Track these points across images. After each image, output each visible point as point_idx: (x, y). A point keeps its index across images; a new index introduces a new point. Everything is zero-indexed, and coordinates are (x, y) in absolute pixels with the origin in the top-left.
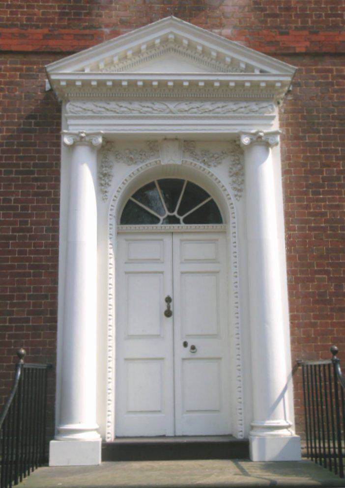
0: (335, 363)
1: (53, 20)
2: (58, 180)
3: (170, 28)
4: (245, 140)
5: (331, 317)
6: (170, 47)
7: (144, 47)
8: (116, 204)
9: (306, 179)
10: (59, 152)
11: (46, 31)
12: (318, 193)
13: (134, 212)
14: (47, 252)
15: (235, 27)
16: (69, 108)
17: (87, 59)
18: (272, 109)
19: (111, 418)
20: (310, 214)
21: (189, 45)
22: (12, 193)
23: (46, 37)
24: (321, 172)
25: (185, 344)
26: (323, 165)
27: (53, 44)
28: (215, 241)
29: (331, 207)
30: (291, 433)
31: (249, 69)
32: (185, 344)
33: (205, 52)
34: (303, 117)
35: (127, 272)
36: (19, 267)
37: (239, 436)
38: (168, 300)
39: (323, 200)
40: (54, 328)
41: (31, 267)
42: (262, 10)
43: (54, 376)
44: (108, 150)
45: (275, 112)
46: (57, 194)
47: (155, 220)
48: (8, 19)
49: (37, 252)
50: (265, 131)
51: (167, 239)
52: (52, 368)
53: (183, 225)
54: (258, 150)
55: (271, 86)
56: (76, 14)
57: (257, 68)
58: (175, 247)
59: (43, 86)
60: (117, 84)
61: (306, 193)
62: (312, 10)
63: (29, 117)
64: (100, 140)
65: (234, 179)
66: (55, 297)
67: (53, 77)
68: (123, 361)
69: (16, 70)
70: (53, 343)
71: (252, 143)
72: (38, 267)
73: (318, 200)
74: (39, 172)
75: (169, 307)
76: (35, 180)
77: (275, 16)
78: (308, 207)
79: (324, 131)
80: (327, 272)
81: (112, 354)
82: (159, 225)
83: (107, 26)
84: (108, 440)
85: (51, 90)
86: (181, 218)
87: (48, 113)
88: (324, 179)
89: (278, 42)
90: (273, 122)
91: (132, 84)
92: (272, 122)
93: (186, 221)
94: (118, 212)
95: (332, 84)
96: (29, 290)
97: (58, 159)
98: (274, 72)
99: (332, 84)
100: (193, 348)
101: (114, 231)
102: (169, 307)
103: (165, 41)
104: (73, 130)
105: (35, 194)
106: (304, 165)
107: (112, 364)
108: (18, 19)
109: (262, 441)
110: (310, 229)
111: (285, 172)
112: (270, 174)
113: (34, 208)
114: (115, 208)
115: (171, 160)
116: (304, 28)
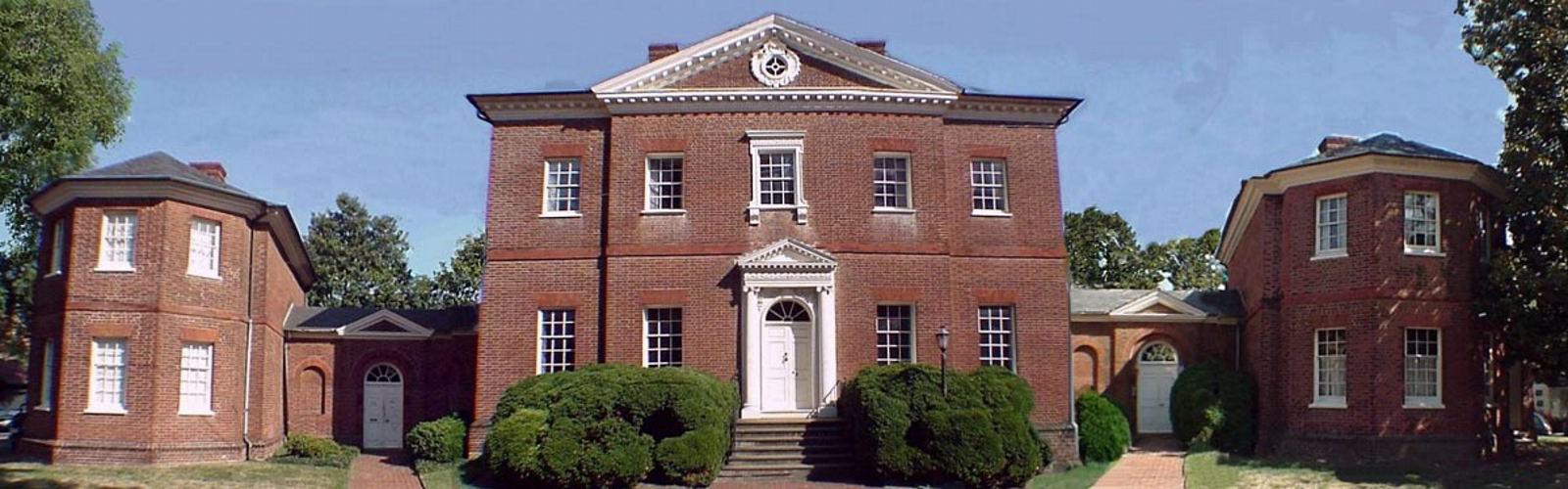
23: (726, 247)
47: (780, 319)
77: (825, 234)
112: (829, 303)
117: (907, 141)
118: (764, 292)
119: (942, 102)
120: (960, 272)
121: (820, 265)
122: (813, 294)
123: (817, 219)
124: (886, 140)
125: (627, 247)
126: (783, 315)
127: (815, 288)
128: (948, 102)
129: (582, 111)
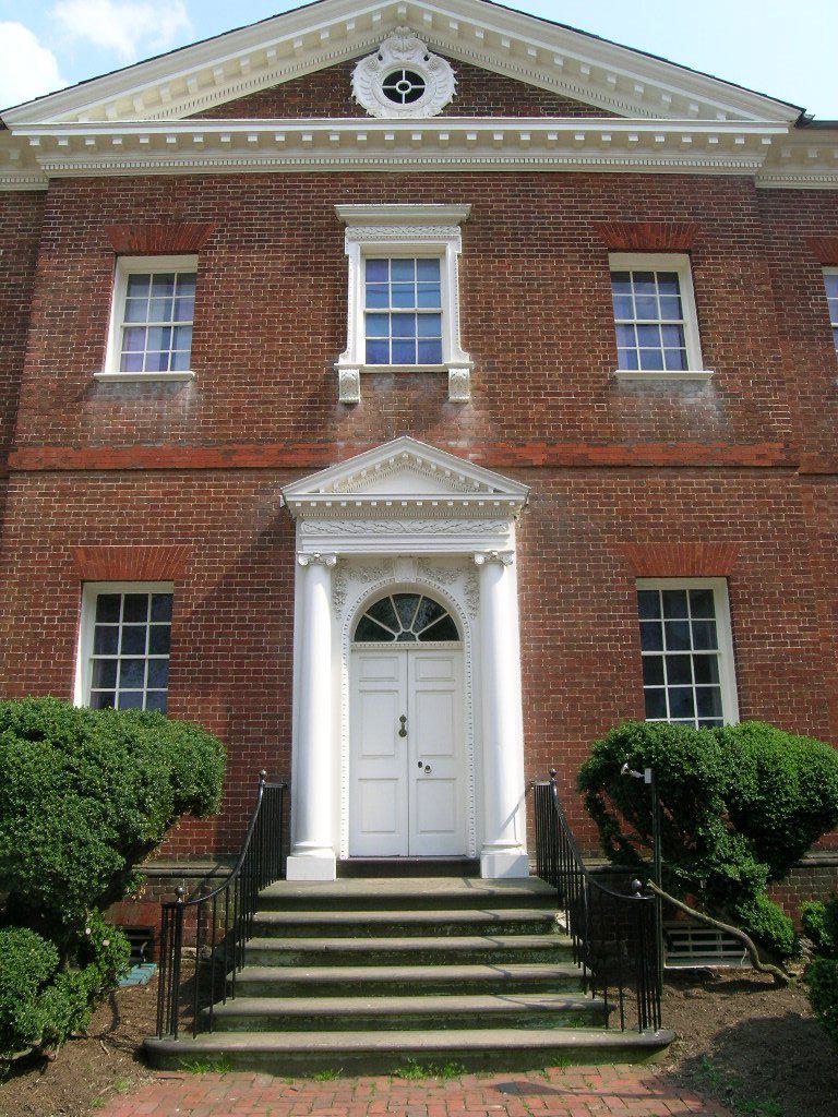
0: (553, 784)
1: (288, 434)
2: (292, 598)
3: (406, 446)
4: (479, 560)
5: (565, 738)
6: (404, 465)
7: (377, 467)
8: (350, 623)
9: (543, 596)
10: (293, 569)
11: (281, 446)
12: (555, 611)
13: (373, 627)
14: (280, 672)
15: (471, 439)
16: (304, 528)
17: (321, 480)
18: (507, 527)
19: (345, 836)
20: (547, 632)
21: (423, 463)
22: (246, 612)
23: (281, 452)
24: (558, 589)
25: (420, 765)
26: (560, 582)
27: (288, 459)
28: (449, 659)
29: (568, 625)
30: (523, 851)
31: (483, 488)
32: (420, 765)
33: (439, 471)
34: (540, 532)
35: (362, 690)
36: (255, 687)
37: (472, 856)
38: (403, 719)
39: (560, 618)
40: (289, 748)
41: (266, 687)
42: (501, 421)
43: (289, 795)
44: (343, 568)
45: (511, 530)
46: (291, 612)
47: (390, 637)
48: (244, 435)
49: (270, 672)
50: (499, 550)
51: (402, 657)
52: (287, 787)
53: (418, 642)
54: (493, 569)
55: (504, 504)
56: (311, 428)
57: (722, 111)
58: (409, 664)
59: (278, 502)
60: (351, 504)
61: (542, 611)
62: (550, 421)
63: (263, 534)
64: (334, 561)
65: (468, 597)
66: (289, 717)
67: (288, 499)
68: (357, 781)
69: (251, 486)
70: (288, 762)
71: (486, 561)
72: (272, 687)
73: (554, 618)
74: (273, 591)
75: (403, 727)
76: (270, 598)
77: (512, 427)
78: (543, 625)
79: (562, 546)
80: (562, 692)
81: (346, 773)
82: (394, 642)
83: (341, 440)
84: (342, 859)
85: (286, 506)
86: (417, 635)
87: (283, 529)
88: (561, 596)
89: (515, 455)
90: (507, 541)
91: (366, 504)
92: (509, 539)
93: (423, 637)
94: (354, 621)
95: (570, 498)
96: (263, 709)
97: (293, 577)
98: (509, 492)
99: (570, 498)
100: (428, 768)
101: (348, 651)
102: (403, 727)
103: (399, 459)
104: (306, 550)
105: (270, 613)
106: (541, 582)
107: (346, 784)
108: (254, 435)
109: (492, 859)
110: (546, 647)
111: (521, 589)
112: (504, 595)
113: (269, 627)
114: (349, 628)
115: (405, 578)
116: (542, 440)
117: (679, 229)
118: (343, 568)
119: (752, 141)
120: (819, 510)
121: (480, 498)
122: (468, 568)
123: (491, 394)
124: (634, 228)
125: (54, 452)
126: (394, 625)
127: (470, 557)
128: (767, 142)
129: (220, 154)
